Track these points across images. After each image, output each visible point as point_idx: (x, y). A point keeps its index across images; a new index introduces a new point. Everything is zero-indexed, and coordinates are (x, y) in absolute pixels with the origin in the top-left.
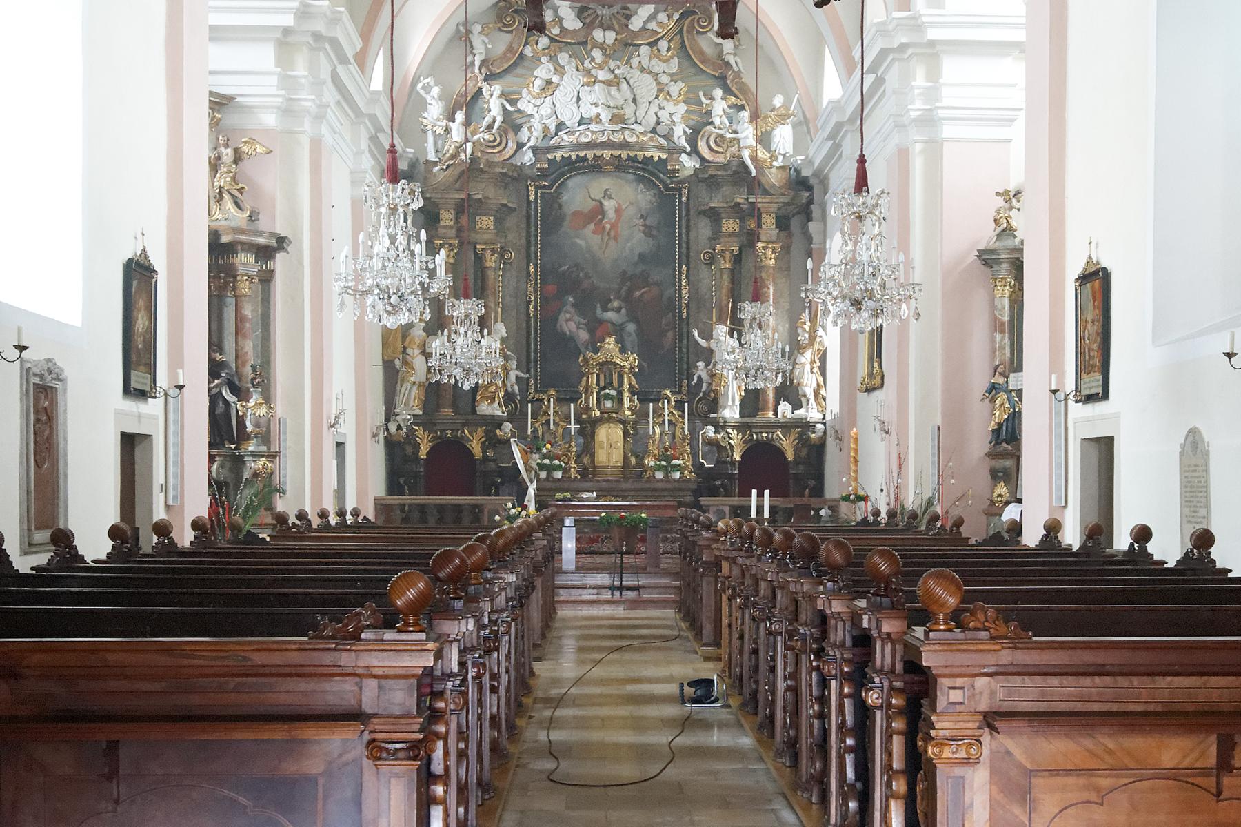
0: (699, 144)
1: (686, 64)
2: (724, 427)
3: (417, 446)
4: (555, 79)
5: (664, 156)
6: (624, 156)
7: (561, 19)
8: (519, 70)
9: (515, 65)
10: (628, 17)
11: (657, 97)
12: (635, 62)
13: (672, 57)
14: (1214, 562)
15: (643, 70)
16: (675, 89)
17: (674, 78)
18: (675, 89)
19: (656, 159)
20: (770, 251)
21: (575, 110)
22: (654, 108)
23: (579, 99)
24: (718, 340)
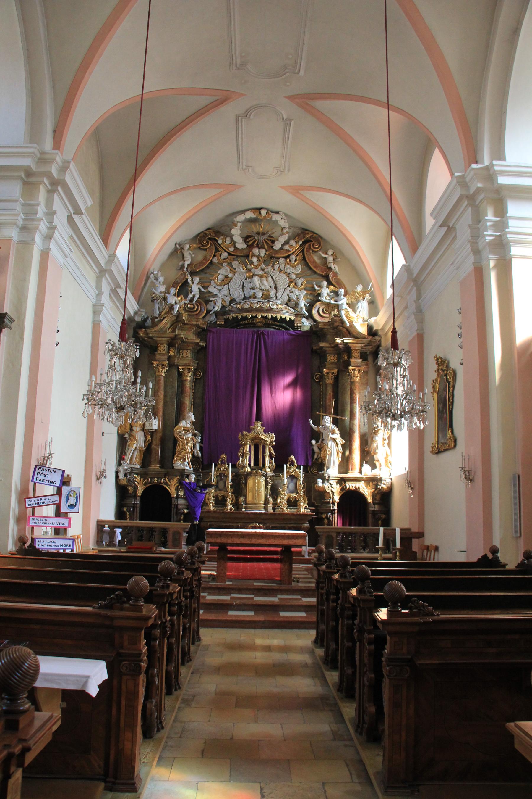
1: (306, 268)
2: (328, 480)
3: (135, 488)
4: (230, 275)
5: (293, 318)
8: (209, 271)
9: (207, 267)
10: (273, 242)
11: (289, 286)
12: (277, 267)
13: (297, 265)
16: (300, 281)
17: (299, 276)
18: (300, 281)
19: (288, 319)
20: (356, 372)
22: (287, 292)
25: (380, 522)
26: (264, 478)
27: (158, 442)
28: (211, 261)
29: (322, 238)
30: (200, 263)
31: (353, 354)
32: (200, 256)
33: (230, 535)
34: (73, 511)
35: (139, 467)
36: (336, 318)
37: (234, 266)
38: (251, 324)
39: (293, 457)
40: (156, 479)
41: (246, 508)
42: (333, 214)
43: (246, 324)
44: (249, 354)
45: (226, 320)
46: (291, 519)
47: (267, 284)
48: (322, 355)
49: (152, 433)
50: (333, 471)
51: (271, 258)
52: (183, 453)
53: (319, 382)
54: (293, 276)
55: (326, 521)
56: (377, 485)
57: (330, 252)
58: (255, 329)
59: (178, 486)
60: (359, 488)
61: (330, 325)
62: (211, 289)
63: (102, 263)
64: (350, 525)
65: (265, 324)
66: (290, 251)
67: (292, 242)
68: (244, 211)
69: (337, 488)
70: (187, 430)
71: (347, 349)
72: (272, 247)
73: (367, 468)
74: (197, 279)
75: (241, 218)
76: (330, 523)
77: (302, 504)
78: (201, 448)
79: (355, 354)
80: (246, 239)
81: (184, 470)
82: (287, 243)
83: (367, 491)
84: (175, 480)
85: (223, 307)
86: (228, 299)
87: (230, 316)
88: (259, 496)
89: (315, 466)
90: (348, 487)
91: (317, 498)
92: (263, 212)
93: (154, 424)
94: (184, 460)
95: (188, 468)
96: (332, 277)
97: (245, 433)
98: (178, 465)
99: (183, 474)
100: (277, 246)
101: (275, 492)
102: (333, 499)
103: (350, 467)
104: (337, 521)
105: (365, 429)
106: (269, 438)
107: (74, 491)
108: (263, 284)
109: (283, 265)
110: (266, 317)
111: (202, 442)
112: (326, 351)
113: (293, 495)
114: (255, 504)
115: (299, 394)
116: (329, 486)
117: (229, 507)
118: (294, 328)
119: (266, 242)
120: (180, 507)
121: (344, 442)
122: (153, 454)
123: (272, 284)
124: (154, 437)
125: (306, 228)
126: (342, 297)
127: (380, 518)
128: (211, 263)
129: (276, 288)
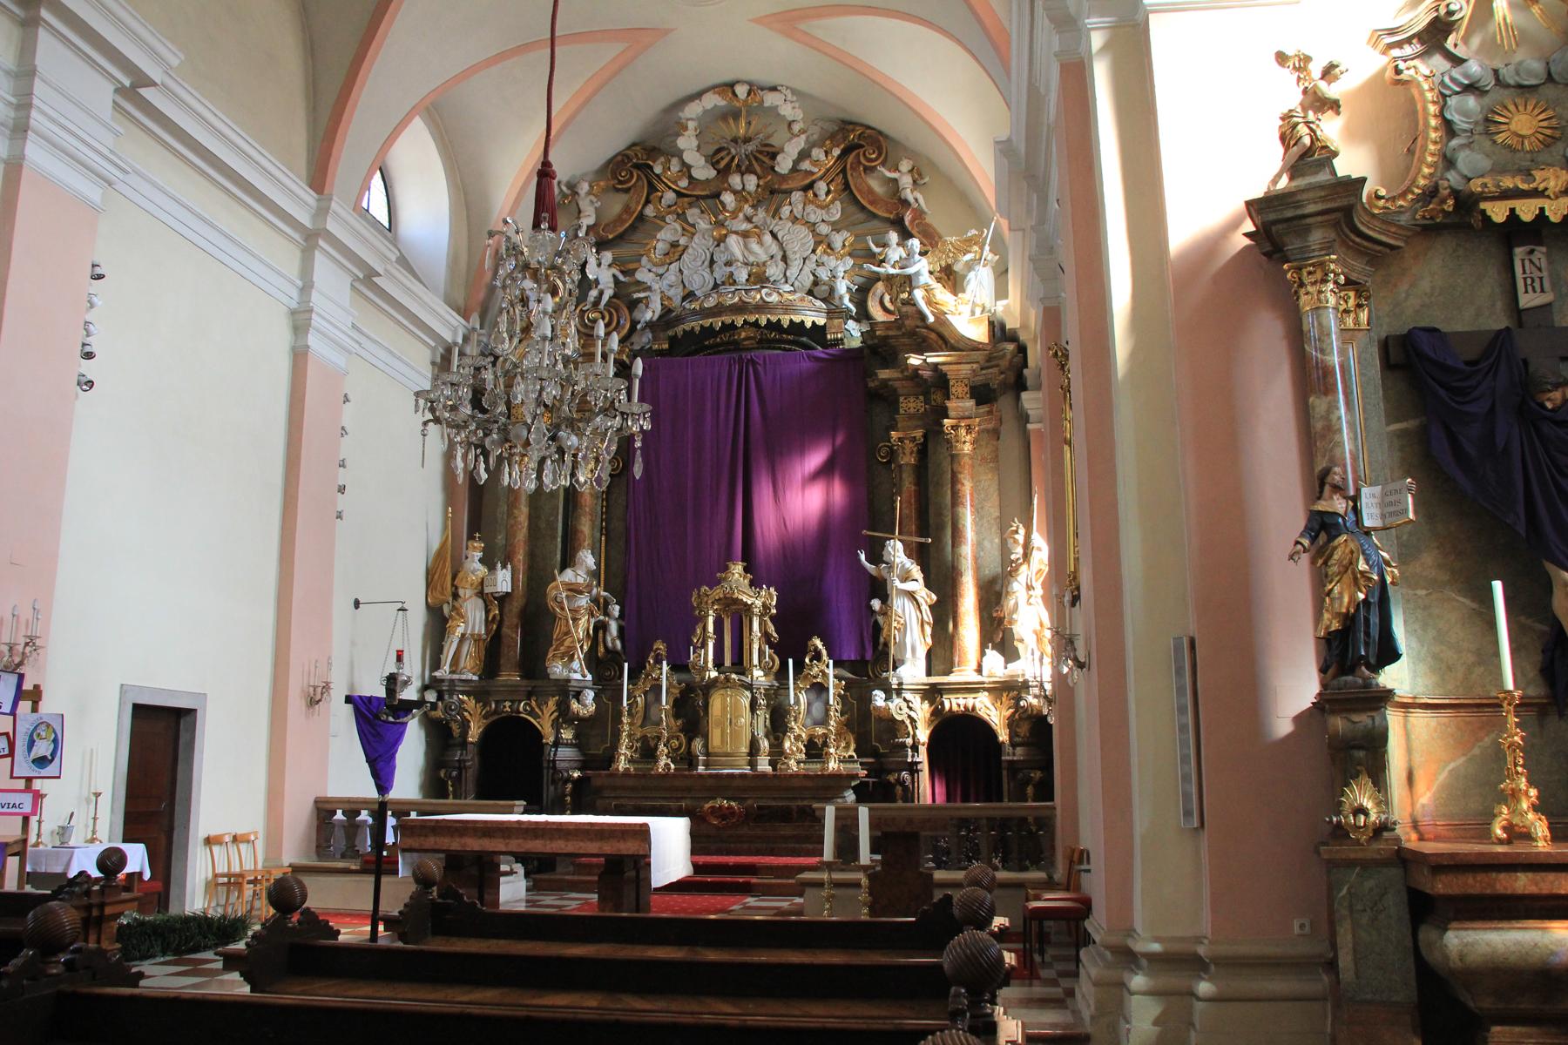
0: (870, 303)
1: (852, 209)
2: (899, 692)
3: (465, 725)
4: (683, 241)
5: (821, 321)
6: (763, 322)
7: (689, 167)
8: (637, 236)
9: (633, 228)
10: (773, 156)
11: (814, 251)
12: (785, 211)
13: (832, 202)
14: (1156, 1023)
15: (795, 220)
16: (838, 240)
17: (836, 227)
18: (838, 240)
19: (808, 325)
20: (963, 432)
21: (707, 275)
22: (811, 265)
23: (712, 262)
24: (890, 566)
25: (1030, 790)
26: (748, 693)
27: (515, 621)
28: (641, 213)
29: (886, 137)
30: (615, 221)
31: (953, 390)
32: (616, 204)
33: (457, 829)
34: (44, 772)
35: (475, 678)
36: (904, 309)
37: (690, 220)
38: (729, 343)
39: (818, 643)
40: (508, 704)
41: (707, 765)
42: (887, 71)
43: (718, 345)
44: (722, 413)
45: (673, 340)
46: (806, 788)
47: (761, 250)
48: (886, 398)
49: (503, 599)
50: (912, 671)
51: (773, 194)
52: (567, 643)
53: (889, 462)
54: (824, 229)
55: (899, 789)
56: (1018, 699)
57: (905, 166)
58: (735, 355)
59: (557, 718)
60: (974, 708)
61: (899, 328)
62: (642, 275)
63: (305, 219)
64: (965, 799)
65: (760, 341)
66: (813, 173)
67: (818, 153)
68: (698, 95)
69: (922, 710)
70: (574, 590)
71: (940, 381)
72: (773, 168)
73: (994, 659)
74: (608, 256)
75: (693, 110)
76: (909, 794)
77: (832, 750)
78: (621, 630)
79: (957, 389)
80: (713, 160)
81: (569, 681)
82: (804, 155)
83: (995, 715)
84: (552, 703)
85: (667, 311)
86: (676, 294)
87: (679, 330)
88: (735, 735)
89: (870, 659)
90: (947, 707)
91: (876, 737)
92: (741, 91)
93: (503, 581)
94: (571, 658)
95: (578, 676)
96: (912, 222)
97: (704, 588)
98: (557, 669)
99: (566, 691)
100: (784, 165)
101: (778, 724)
102: (914, 736)
103: (956, 660)
104: (927, 789)
105: (992, 566)
106: (763, 600)
107: (48, 725)
108: (751, 252)
109: (800, 207)
110: (756, 324)
111: (622, 616)
112: (895, 390)
113: (820, 731)
114: (727, 755)
115: (838, 492)
116: (904, 705)
117: (662, 763)
118: (825, 344)
119: (756, 159)
120: (560, 765)
121: (934, 597)
122: (504, 650)
123: (774, 249)
124: (506, 610)
125: (847, 117)
126: (917, 257)
127: (1028, 781)
128: (641, 217)
129: (785, 259)
